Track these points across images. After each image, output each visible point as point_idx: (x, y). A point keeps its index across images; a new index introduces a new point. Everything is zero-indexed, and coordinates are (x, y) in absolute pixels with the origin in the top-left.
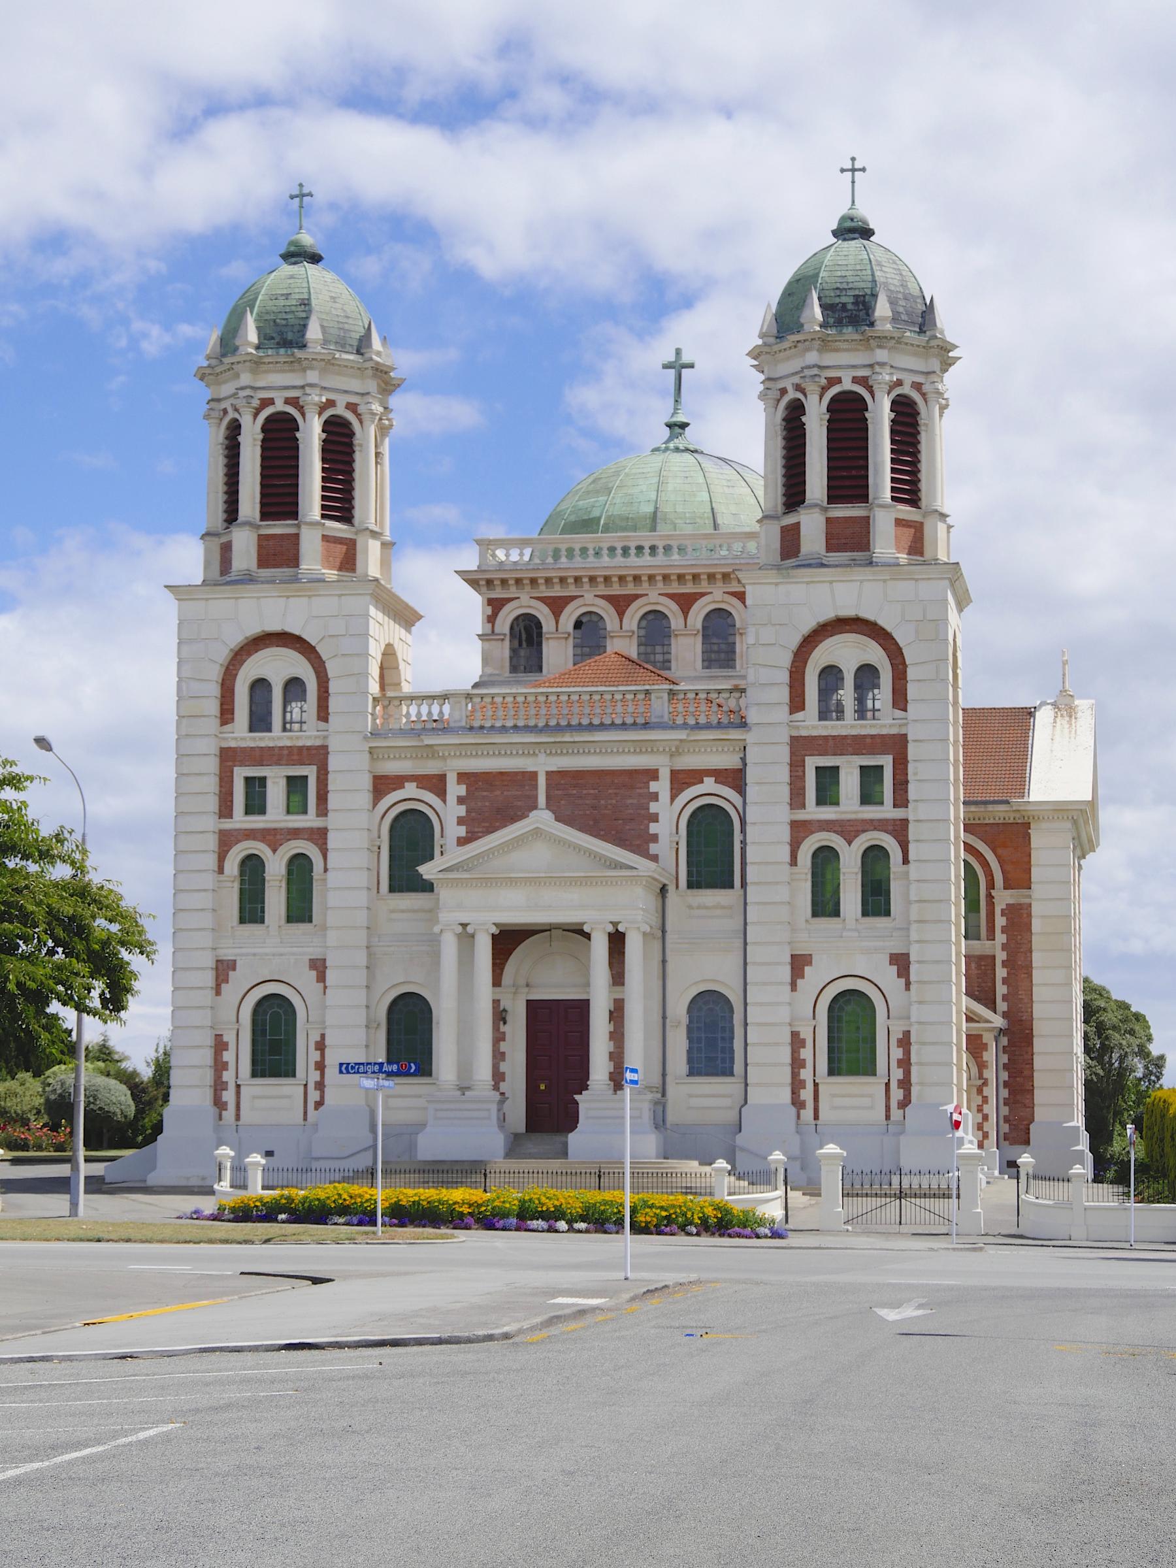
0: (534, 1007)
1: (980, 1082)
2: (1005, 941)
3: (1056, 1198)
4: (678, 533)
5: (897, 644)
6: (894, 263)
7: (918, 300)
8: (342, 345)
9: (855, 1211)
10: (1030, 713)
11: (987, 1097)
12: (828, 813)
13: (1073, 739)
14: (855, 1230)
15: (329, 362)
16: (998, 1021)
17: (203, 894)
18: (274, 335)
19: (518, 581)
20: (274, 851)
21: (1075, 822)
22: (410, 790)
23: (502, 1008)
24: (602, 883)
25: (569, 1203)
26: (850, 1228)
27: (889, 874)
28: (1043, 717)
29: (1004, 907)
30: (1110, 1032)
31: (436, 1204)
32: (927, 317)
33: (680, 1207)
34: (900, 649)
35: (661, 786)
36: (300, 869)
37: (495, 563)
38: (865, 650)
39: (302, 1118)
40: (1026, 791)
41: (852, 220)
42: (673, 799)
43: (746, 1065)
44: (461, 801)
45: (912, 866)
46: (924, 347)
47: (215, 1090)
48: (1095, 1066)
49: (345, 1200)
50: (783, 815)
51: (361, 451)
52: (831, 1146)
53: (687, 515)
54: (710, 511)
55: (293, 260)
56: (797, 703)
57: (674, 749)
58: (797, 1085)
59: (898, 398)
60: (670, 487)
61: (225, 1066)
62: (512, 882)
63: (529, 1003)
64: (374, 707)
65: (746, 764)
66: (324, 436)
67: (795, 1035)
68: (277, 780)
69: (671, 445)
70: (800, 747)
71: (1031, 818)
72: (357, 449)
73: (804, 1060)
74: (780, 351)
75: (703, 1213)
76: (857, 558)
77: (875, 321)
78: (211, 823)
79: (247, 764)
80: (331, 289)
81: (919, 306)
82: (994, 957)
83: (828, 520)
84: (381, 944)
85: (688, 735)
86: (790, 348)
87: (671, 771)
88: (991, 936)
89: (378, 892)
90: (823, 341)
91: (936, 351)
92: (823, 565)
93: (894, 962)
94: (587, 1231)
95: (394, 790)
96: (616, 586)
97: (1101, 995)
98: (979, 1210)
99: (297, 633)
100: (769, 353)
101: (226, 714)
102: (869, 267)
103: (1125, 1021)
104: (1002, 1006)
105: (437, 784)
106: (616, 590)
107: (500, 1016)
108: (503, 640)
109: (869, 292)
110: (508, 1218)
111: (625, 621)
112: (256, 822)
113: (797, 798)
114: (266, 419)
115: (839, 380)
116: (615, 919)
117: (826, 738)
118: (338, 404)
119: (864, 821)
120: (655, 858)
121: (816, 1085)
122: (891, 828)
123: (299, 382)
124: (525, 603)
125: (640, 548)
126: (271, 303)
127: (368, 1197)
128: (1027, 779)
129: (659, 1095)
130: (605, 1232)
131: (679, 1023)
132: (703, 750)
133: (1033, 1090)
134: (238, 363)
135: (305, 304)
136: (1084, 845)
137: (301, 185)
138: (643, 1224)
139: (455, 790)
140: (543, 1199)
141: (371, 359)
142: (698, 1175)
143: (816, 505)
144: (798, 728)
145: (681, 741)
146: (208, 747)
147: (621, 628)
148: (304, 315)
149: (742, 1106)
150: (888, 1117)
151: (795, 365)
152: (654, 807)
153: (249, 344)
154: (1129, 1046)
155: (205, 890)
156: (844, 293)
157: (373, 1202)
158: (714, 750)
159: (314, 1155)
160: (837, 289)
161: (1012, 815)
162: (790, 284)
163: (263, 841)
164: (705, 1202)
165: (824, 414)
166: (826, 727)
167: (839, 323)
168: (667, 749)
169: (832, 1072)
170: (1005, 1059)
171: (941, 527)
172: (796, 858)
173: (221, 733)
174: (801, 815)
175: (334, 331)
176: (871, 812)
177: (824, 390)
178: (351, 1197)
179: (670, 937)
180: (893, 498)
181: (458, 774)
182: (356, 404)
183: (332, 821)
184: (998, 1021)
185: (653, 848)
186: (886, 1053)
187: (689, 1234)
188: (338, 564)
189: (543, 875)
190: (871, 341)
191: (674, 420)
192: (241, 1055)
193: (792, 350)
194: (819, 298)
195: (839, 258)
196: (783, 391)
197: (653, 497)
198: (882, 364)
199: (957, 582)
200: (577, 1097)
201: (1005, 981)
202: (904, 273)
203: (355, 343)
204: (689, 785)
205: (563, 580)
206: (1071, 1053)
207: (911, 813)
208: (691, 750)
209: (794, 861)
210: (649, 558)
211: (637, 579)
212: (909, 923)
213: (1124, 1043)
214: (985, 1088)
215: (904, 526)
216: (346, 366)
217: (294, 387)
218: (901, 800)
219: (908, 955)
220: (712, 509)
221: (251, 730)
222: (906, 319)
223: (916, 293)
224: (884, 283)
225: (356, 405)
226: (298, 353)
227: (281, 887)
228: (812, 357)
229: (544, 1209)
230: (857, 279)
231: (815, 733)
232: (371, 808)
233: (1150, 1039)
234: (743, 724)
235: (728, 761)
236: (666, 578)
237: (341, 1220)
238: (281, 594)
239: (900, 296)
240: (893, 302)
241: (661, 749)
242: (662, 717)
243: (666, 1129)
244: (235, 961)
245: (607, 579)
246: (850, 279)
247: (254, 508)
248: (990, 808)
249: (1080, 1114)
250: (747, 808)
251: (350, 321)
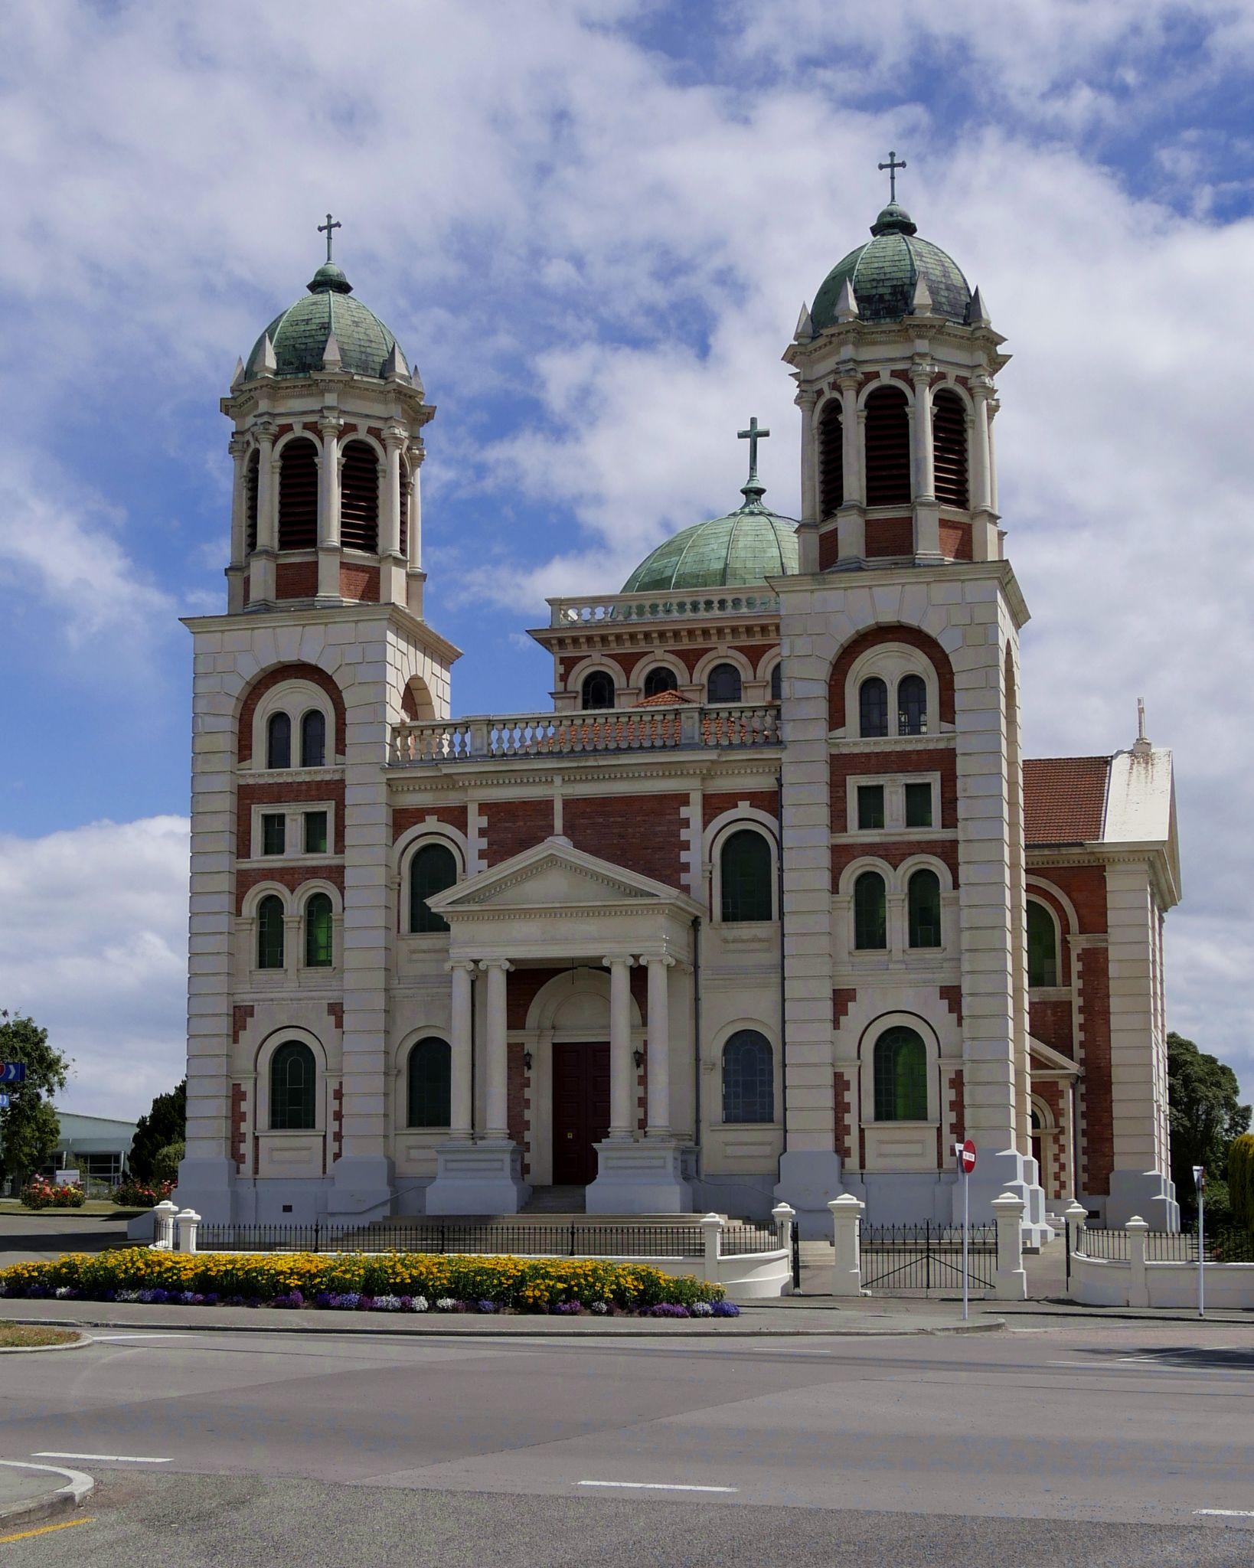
0: (560, 1051)
1: (1057, 1131)
2: (1081, 987)
3: (1111, 1256)
4: (747, 585)
5: (943, 651)
6: (936, 254)
7: (962, 292)
8: (364, 367)
9: (880, 1271)
10: (1105, 762)
11: (1063, 1145)
12: (871, 836)
13: (1149, 784)
14: (875, 1295)
15: (346, 384)
16: (1074, 1068)
17: (218, 936)
18: (293, 360)
19: (589, 639)
20: (292, 891)
21: (1152, 865)
22: (431, 823)
23: (526, 1052)
24: (621, 912)
25: (432, 1273)
26: (869, 1292)
27: (939, 901)
28: (1119, 766)
29: (1080, 952)
30: (1197, 1084)
31: (254, 1274)
32: (972, 308)
33: (586, 1276)
34: (946, 656)
35: (693, 812)
37: (567, 622)
38: (910, 660)
39: (321, 1171)
40: (1101, 833)
41: (891, 214)
42: (705, 824)
43: (785, 1109)
44: (482, 833)
45: (962, 889)
46: (968, 339)
47: (233, 1142)
48: (1182, 1118)
49: (139, 1269)
50: (823, 838)
51: (384, 477)
52: (847, 1196)
53: (757, 570)
54: (779, 565)
55: (319, 289)
56: (836, 719)
57: (705, 772)
58: (840, 1131)
59: (942, 393)
60: (741, 544)
61: (242, 1117)
62: (527, 913)
63: (554, 1045)
64: (394, 738)
65: (782, 785)
66: (343, 461)
67: (838, 1077)
68: (295, 817)
69: (747, 510)
70: (841, 766)
71: (1106, 860)
72: (380, 475)
73: (849, 1104)
74: (815, 350)
75: (618, 1284)
76: (900, 561)
77: (914, 310)
78: (225, 863)
79: (265, 801)
80: (354, 314)
81: (963, 298)
82: (1070, 1003)
83: (868, 523)
84: (401, 986)
85: (719, 756)
86: (825, 345)
87: (704, 795)
88: (1067, 982)
89: (399, 932)
90: (858, 333)
91: (981, 342)
92: (860, 569)
93: (945, 996)
94: (454, 1310)
95: (415, 824)
96: (686, 640)
97: (1187, 1050)
98: (1021, 1271)
99: (313, 662)
100: (805, 353)
101: (244, 750)
102: (908, 257)
103: (1212, 1073)
104: (1079, 1053)
105: (457, 817)
106: (686, 644)
107: (519, 1060)
108: (575, 698)
109: (907, 281)
110: (348, 1293)
112: (275, 861)
113: (838, 821)
114: (284, 446)
115: (876, 375)
116: (636, 951)
117: (868, 755)
118: (359, 428)
119: (910, 843)
120: (686, 889)
121: (862, 1131)
122: (939, 850)
124: (596, 661)
125: (709, 604)
126: (291, 329)
127: (169, 1264)
128: (1102, 822)
129: (692, 1144)
130: (480, 1311)
131: (714, 1065)
132: (736, 772)
133: (1112, 1138)
134: (256, 389)
135: (325, 328)
136: (1165, 898)
137: (329, 217)
138: (531, 1300)
140: (399, 1268)
141: (394, 381)
142: (732, 1230)
143: (853, 507)
144: (837, 745)
145: (712, 762)
146: (224, 783)
147: (691, 682)
148: (323, 338)
149: (781, 1155)
150: (940, 1165)
151: (829, 364)
152: (684, 835)
153: (267, 369)
154: (1216, 1097)
155: (221, 933)
156: (881, 284)
157: (175, 1271)
158: (749, 771)
159: (330, 1210)
160: (873, 280)
161: (1086, 858)
162: (826, 283)
163: (281, 882)
164: (624, 1270)
165: (862, 411)
166: (868, 744)
167: (876, 315)
168: (698, 772)
169: (879, 1116)
170: (1083, 1107)
171: (992, 531)
172: (838, 885)
173: (239, 770)
174: (842, 839)
175: (356, 355)
176: (918, 834)
177: (861, 386)
178: (147, 1265)
179: (703, 974)
180: (937, 497)
181: (480, 804)
182: (378, 429)
183: (350, 858)
184: (1074, 1068)
185: (685, 879)
186: (937, 1095)
187: (597, 1313)
188: (359, 593)
189: (558, 905)
190: (911, 330)
191: (750, 486)
192: (259, 1105)
193: (827, 348)
194: (855, 291)
195: (877, 250)
196: (820, 393)
197: (724, 553)
198: (922, 355)
199: (1009, 586)
200: (595, 1145)
201: (1082, 1027)
202: (946, 264)
203: (378, 367)
204: (723, 810)
205: (633, 637)
206: (1149, 1100)
207: (960, 833)
208: (724, 773)
209: (835, 889)
210: (718, 612)
211: (706, 633)
212: (960, 952)
213: (1210, 1095)
214: (1061, 1137)
215: (950, 527)
216: (367, 390)
217: (312, 412)
218: (950, 820)
219: (959, 987)
220: (782, 564)
221: (270, 766)
222: (949, 309)
223: (960, 284)
224: (924, 272)
225: (380, 430)
226: (315, 375)
227: (299, 928)
228: (848, 352)
229: (398, 1280)
230: (895, 269)
231: (856, 750)
232: (390, 844)
233: (1236, 1092)
234: (779, 743)
235: (762, 783)
236: (734, 630)
237: (134, 1296)
238: (296, 623)
239: (943, 286)
240: (933, 291)
241: (691, 772)
242: (693, 738)
243: (700, 1181)
244: (253, 1006)
245: (676, 634)
246: (888, 270)
247: (272, 539)
248: (1064, 851)
249: (1163, 1164)
250: (784, 832)
251: (373, 345)
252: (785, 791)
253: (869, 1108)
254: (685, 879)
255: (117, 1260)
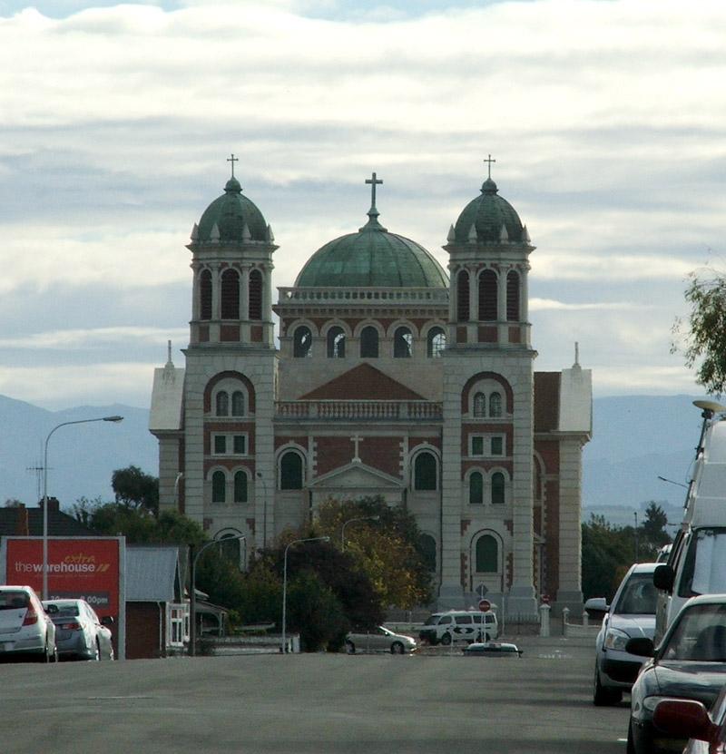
12: (477, 457)
35: (405, 445)
36: (240, 480)
44: (315, 449)
58: (463, 576)
105: (304, 441)
111: (355, 332)
113: (464, 451)
115: (484, 265)
123: (240, 256)
139: (312, 444)
167: (485, 239)
170: (544, 558)
176: (497, 457)
183: (258, 457)
185: (401, 473)
206: (577, 555)
218: (510, 452)
219: (512, 521)
245: (346, 311)
252: (444, 439)
253: (474, 567)
254: (401, 473)
255: (369, 567)
